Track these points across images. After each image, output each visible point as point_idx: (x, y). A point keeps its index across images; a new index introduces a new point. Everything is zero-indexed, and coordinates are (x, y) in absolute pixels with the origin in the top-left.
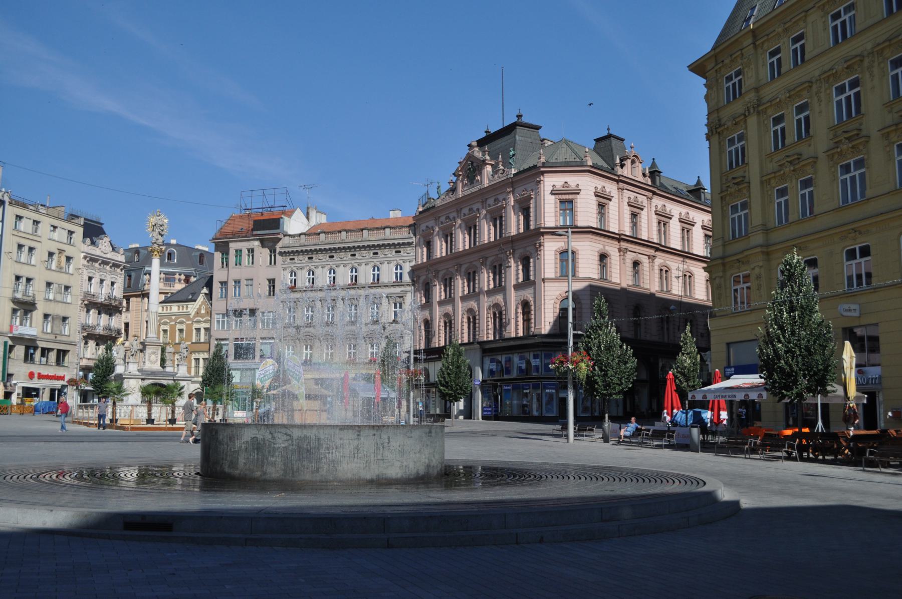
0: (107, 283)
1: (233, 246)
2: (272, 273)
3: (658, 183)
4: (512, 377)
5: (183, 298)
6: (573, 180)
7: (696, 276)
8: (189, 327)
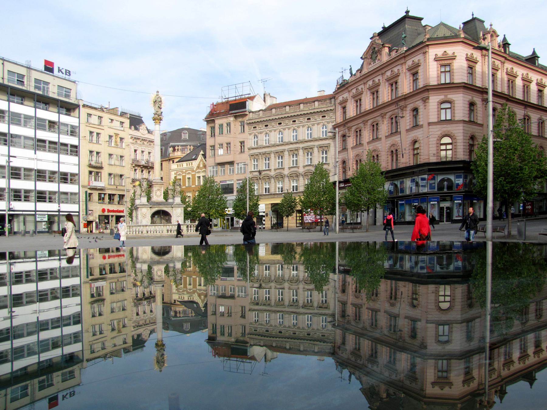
0: (146, 153)
2: (242, 137)
3: (507, 53)
4: (393, 196)
5: (190, 159)
6: (450, 50)
7: (532, 119)
8: (194, 176)
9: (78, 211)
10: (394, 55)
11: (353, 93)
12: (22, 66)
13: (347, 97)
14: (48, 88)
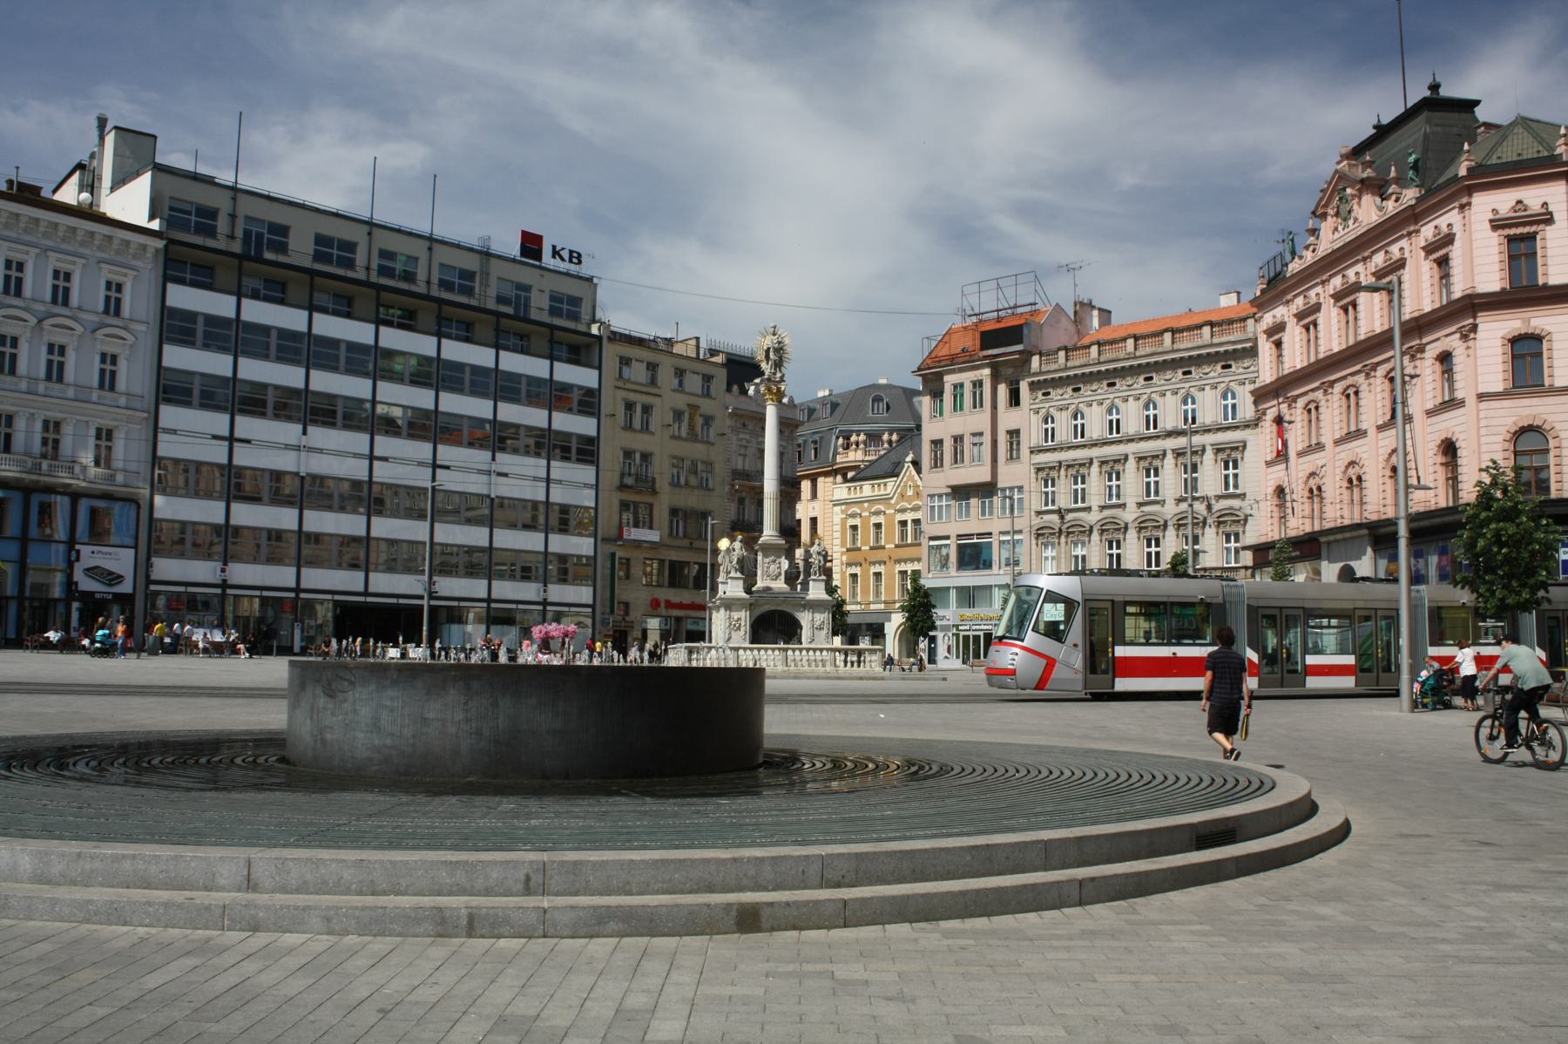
1: (950, 380)
9: (590, 602)
10: (1390, 208)
11: (1298, 305)
12: (471, 250)
13: (1283, 315)
14: (528, 299)
